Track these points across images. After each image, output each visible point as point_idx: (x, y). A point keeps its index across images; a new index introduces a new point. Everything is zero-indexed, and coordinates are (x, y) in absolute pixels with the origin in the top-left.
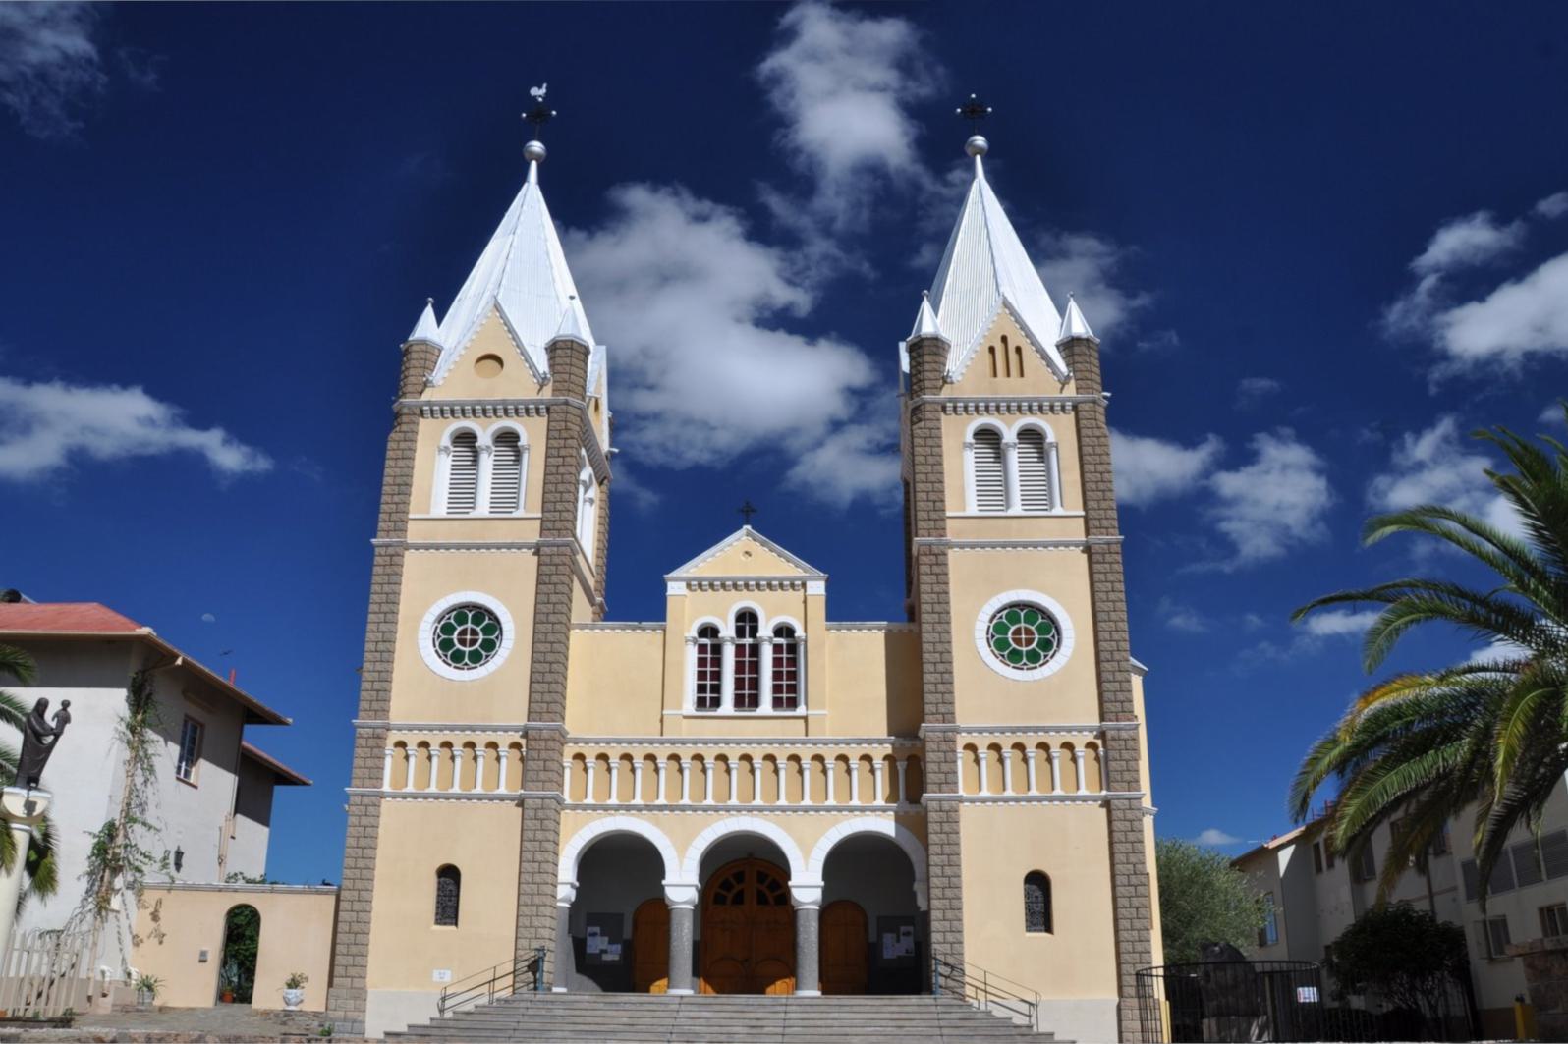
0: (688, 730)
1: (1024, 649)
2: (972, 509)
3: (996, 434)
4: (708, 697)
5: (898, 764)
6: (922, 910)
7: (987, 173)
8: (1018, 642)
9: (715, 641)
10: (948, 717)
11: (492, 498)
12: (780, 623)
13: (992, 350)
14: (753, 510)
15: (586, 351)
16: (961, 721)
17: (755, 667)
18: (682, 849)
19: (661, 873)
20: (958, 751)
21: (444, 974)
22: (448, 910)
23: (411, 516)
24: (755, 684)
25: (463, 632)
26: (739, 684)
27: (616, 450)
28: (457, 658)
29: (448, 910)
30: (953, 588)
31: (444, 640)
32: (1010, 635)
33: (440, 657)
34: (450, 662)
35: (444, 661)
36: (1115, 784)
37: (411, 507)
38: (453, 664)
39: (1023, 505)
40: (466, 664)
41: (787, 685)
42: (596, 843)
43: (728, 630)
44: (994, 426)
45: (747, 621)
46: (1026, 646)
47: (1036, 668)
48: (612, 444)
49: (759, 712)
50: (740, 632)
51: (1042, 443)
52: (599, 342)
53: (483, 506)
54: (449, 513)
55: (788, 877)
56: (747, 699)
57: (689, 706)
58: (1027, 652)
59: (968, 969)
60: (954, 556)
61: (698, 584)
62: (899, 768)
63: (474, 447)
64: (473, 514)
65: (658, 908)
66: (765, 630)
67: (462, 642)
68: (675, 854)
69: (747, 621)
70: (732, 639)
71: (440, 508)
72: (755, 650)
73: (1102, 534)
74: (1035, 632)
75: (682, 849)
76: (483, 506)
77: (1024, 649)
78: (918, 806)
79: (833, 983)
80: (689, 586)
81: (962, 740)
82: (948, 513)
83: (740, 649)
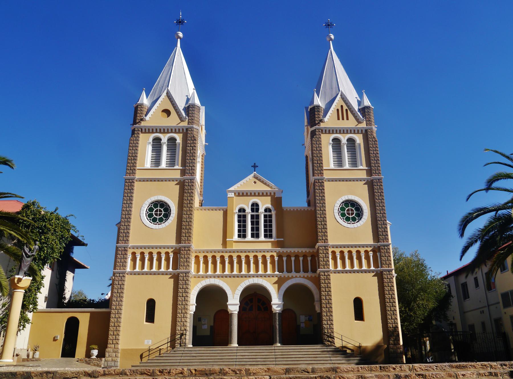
0: (235, 247)
1: (351, 216)
2: (332, 166)
3: (340, 140)
4: (242, 234)
5: (308, 258)
6: (317, 312)
7: (181, 47)
8: (348, 214)
9: (257, 213)
10: (326, 241)
11: (151, 161)
12: (240, 207)
13: (338, 110)
14: (255, 165)
15: (199, 109)
16: (330, 243)
17: (258, 223)
18: (234, 292)
19: (226, 300)
20: (329, 253)
21: (149, 341)
22: (150, 317)
23: (137, 168)
24: (258, 229)
25: (157, 211)
26: (252, 229)
27: (207, 144)
28: (154, 220)
29: (150, 317)
30: (326, 195)
31: (150, 213)
32: (346, 212)
33: (148, 220)
34: (152, 222)
35: (150, 221)
36: (383, 265)
37: (137, 165)
38: (153, 223)
39: (334, 165)
40: (158, 223)
41: (243, 229)
42: (202, 289)
43: (248, 210)
44: (339, 137)
45: (255, 207)
46: (351, 215)
47: (355, 223)
48: (206, 142)
49: (246, 239)
50: (252, 210)
51: (340, 143)
52: (202, 105)
53: (164, 164)
54: (151, 167)
55: (271, 301)
56: (255, 234)
57: (236, 237)
58: (351, 217)
59: (335, 335)
60: (326, 184)
61: (240, 194)
62: (308, 259)
63: (161, 143)
64: (160, 168)
65: (226, 315)
66: (262, 210)
67: (156, 215)
68: (231, 293)
69: (255, 207)
70: (250, 213)
71: (148, 164)
72: (258, 217)
73: (376, 176)
74: (163, 211)
75: (234, 292)
76: (164, 164)
77: (351, 216)
78: (315, 273)
79: (284, 342)
80: (235, 194)
81: (330, 250)
82: (324, 168)
83: (252, 217)
